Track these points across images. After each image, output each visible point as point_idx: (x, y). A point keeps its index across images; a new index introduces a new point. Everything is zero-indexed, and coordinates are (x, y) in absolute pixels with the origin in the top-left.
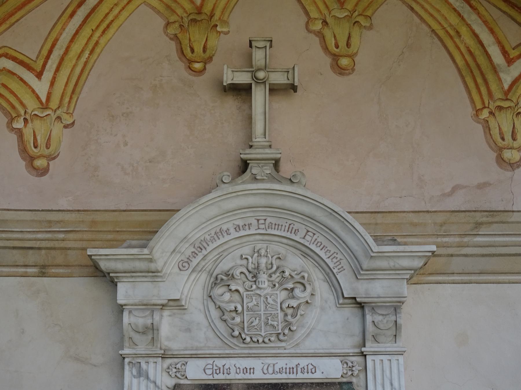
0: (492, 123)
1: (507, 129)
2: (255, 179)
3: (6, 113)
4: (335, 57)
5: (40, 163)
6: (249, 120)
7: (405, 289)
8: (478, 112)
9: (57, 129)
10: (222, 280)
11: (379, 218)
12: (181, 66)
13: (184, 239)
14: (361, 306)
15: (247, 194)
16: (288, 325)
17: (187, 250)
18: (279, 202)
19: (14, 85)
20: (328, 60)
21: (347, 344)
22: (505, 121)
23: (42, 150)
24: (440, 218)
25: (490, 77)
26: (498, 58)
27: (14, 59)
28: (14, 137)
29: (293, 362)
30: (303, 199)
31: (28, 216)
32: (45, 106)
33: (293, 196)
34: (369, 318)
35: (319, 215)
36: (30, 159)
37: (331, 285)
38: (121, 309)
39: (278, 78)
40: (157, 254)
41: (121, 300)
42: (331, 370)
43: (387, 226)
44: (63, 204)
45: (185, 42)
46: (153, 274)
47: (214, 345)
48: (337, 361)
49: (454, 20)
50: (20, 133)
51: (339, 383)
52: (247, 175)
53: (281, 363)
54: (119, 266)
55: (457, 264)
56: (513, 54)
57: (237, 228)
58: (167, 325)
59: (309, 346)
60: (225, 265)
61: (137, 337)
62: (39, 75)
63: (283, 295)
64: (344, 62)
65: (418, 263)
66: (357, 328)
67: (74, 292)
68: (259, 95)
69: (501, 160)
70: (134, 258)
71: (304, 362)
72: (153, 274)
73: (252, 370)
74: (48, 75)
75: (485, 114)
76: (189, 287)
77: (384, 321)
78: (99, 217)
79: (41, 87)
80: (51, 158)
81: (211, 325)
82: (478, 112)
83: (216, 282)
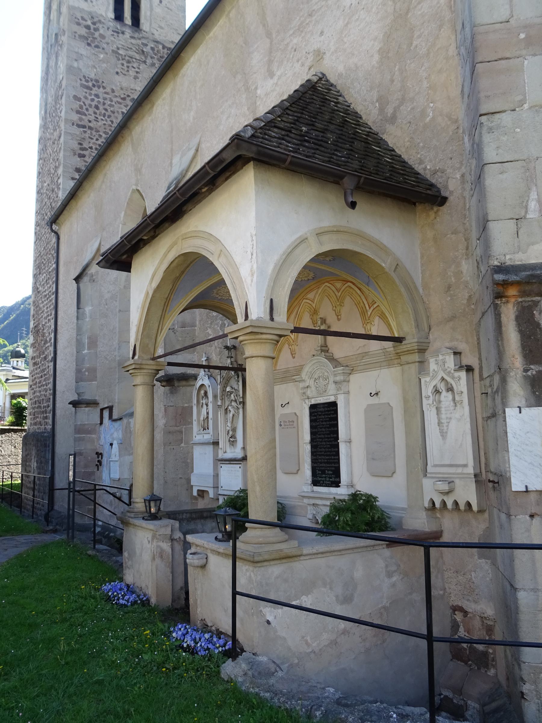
1: (369, 329)
8: (363, 325)
20: (336, 317)
24: (356, 356)
36: (292, 355)
40: (302, 376)
49: (359, 298)
53: (325, 398)
56: (371, 305)
71: (328, 397)
73: (320, 400)
82: (363, 325)
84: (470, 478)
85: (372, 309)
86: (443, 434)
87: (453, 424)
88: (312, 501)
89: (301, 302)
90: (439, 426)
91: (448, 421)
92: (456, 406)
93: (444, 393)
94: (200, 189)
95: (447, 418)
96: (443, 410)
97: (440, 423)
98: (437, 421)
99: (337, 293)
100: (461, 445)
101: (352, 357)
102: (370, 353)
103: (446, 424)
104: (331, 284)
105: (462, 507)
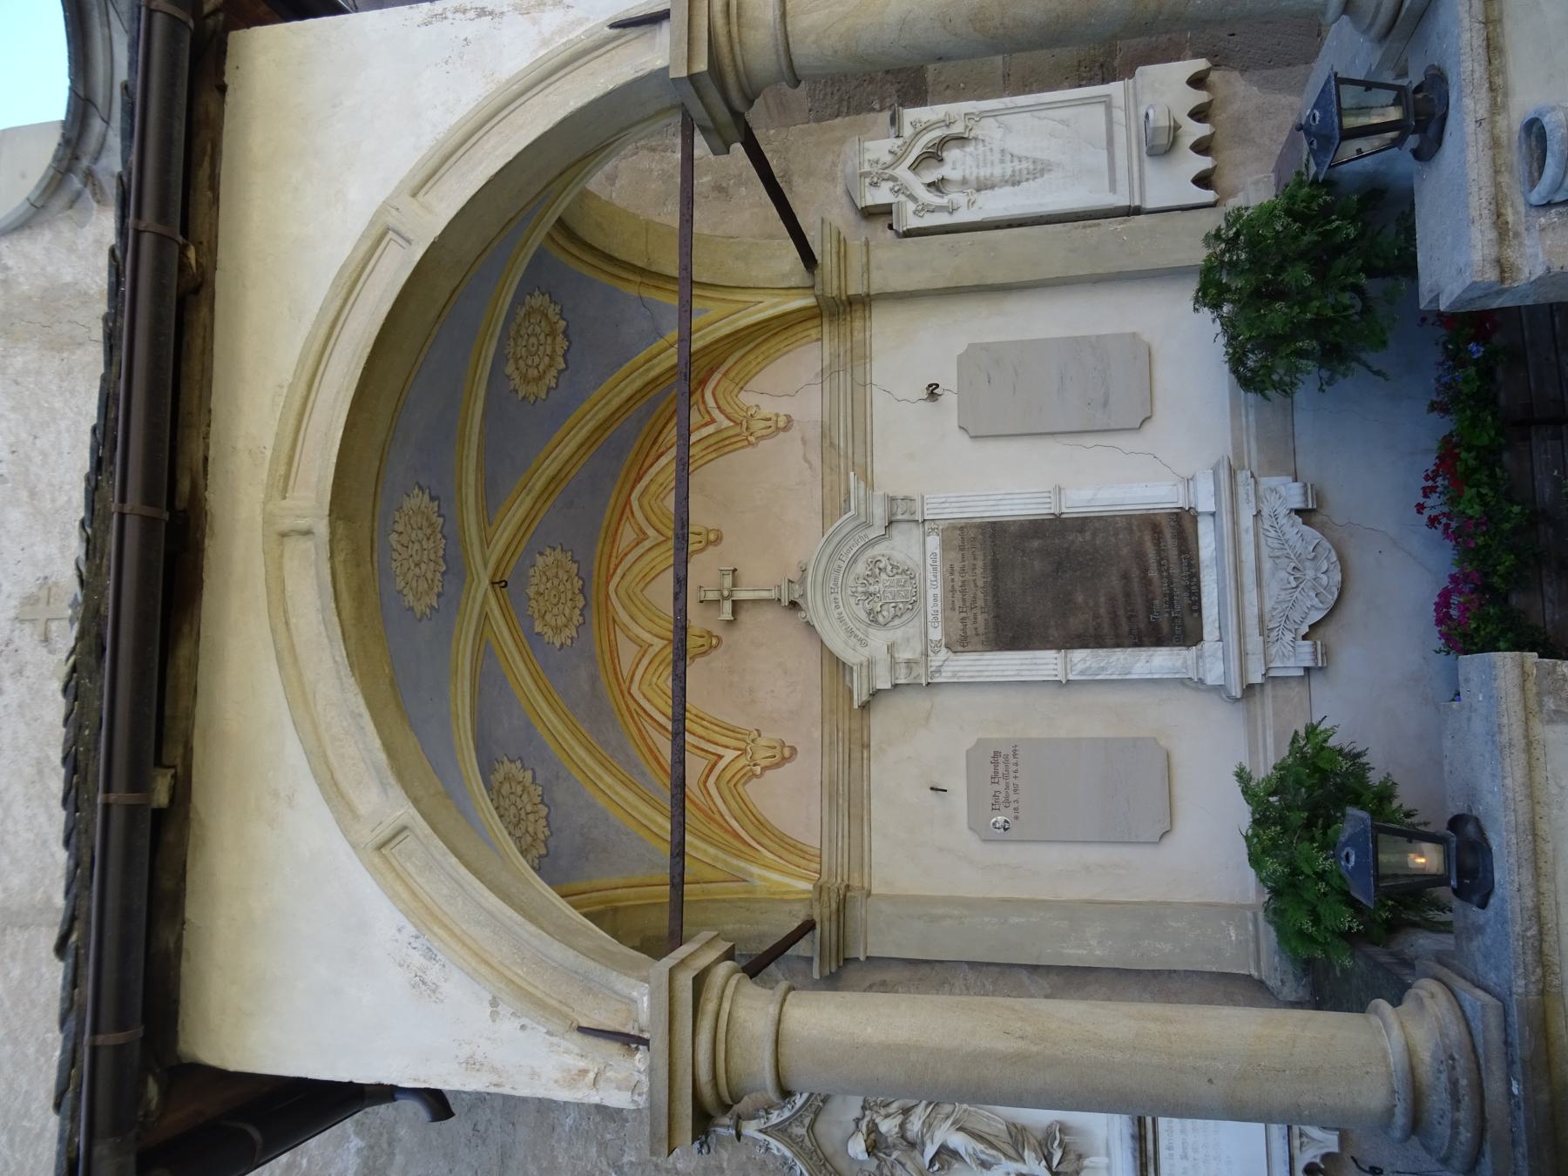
0: (759, 434)
1: (763, 424)
2: (803, 596)
3: (750, 779)
4: (709, 543)
5: (787, 753)
6: (755, 601)
7: (879, 493)
8: (750, 444)
9: (762, 742)
10: (873, 618)
11: (827, 512)
12: (714, 653)
13: (846, 643)
14: (891, 523)
15: (816, 607)
16: (904, 572)
17: (853, 641)
18: (820, 579)
19: (728, 775)
20: (711, 548)
21: (917, 532)
22: (758, 426)
23: (777, 752)
24: (827, 471)
25: (725, 434)
26: (711, 429)
27: (708, 776)
28: (768, 773)
29: (929, 568)
30: (818, 561)
31: (826, 759)
32: (744, 751)
33: (816, 569)
34: (899, 517)
35: (829, 550)
36: (784, 760)
37: (876, 543)
38: (895, 686)
39: (728, 581)
40: (856, 661)
41: (889, 686)
42: (934, 542)
43: (835, 505)
44: (817, 734)
45: (697, 651)
46: (871, 663)
47: (918, 622)
48: (928, 539)
50: (764, 769)
51: (1437, 81)
52: (800, 601)
53: (930, 576)
54: (865, 686)
55: (859, 460)
56: (707, 418)
57: (837, 607)
58: (904, 655)
59: (918, 557)
60: (863, 616)
61: (914, 674)
62: (721, 757)
63: (883, 576)
64: (712, 537)
65: (862, 484)
66: (905, 526)
67: (881, 723)
68: (741, 595)
69: (786, 429)
70: (860, 676)
71: (929, 561)
72: (871, 663)
74: (720, 751)
75: (752, 439)
76: (878, 640)
77: (901, 507)
78: (826, 708)
79: (729, 755)
80: (783, 744)
81: (904, 624)
82: (750, 444)
83: (875, 621)
84: (1135, 88)
85: (716, 413)
86: (1040, 169)
87: (1016, 145)
88: (1254, 641)
89: (633, 706)
90: (1019, 183)
91: (1008, 157)
92: (976, 139)
93: (945, 171)
94: (183, 266)
95: (1002, 161)
96: (984, 172)
97: (1015, 182)
98: (1008, 189)
99: (647, 544)
100: (1062, 122)
101: (827, 488)
102: (826, 420)
103: (1016, 162)
104: (617, 566)
105: (1201, 97)
